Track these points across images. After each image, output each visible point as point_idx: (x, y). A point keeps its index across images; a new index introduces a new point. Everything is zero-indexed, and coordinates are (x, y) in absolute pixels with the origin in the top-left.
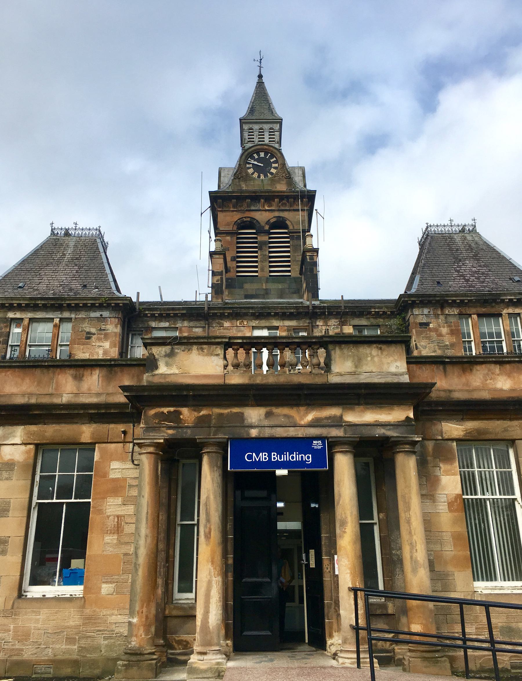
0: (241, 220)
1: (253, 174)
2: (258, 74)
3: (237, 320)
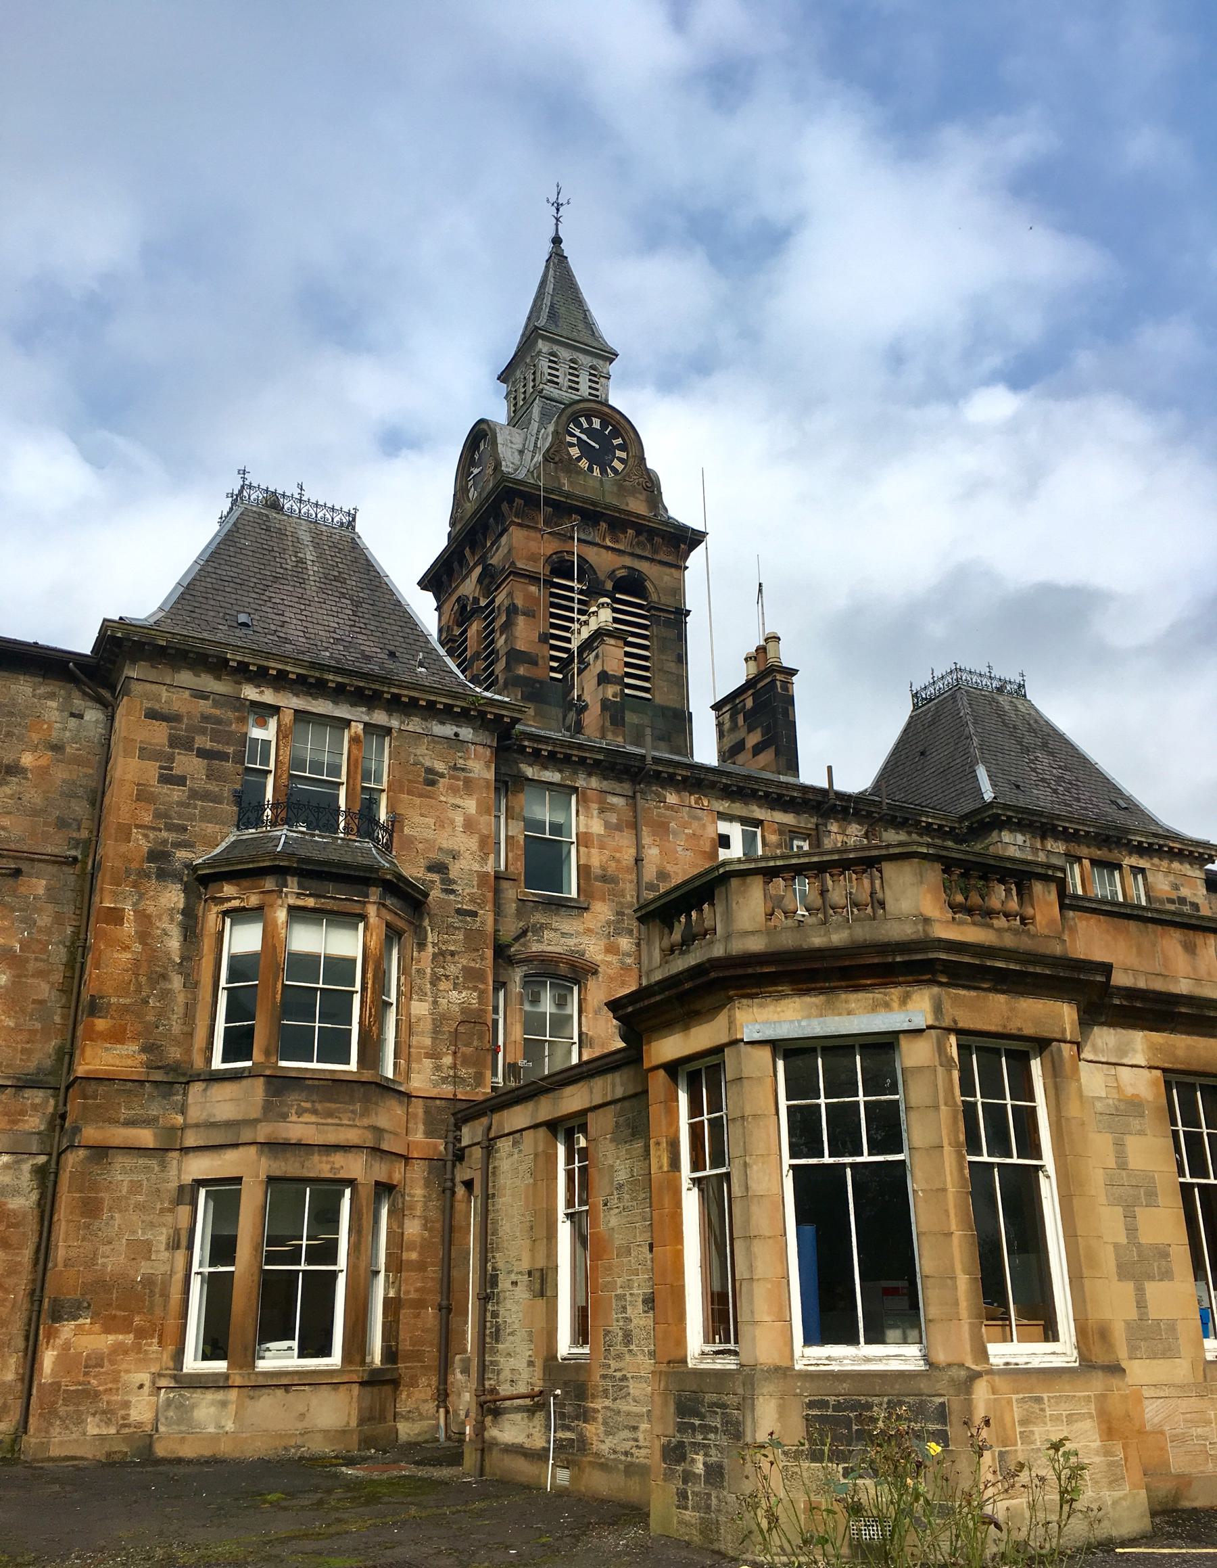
0: (559, 555)
1: (579, 459)
2: (553, 234)
3: (691, 794)
